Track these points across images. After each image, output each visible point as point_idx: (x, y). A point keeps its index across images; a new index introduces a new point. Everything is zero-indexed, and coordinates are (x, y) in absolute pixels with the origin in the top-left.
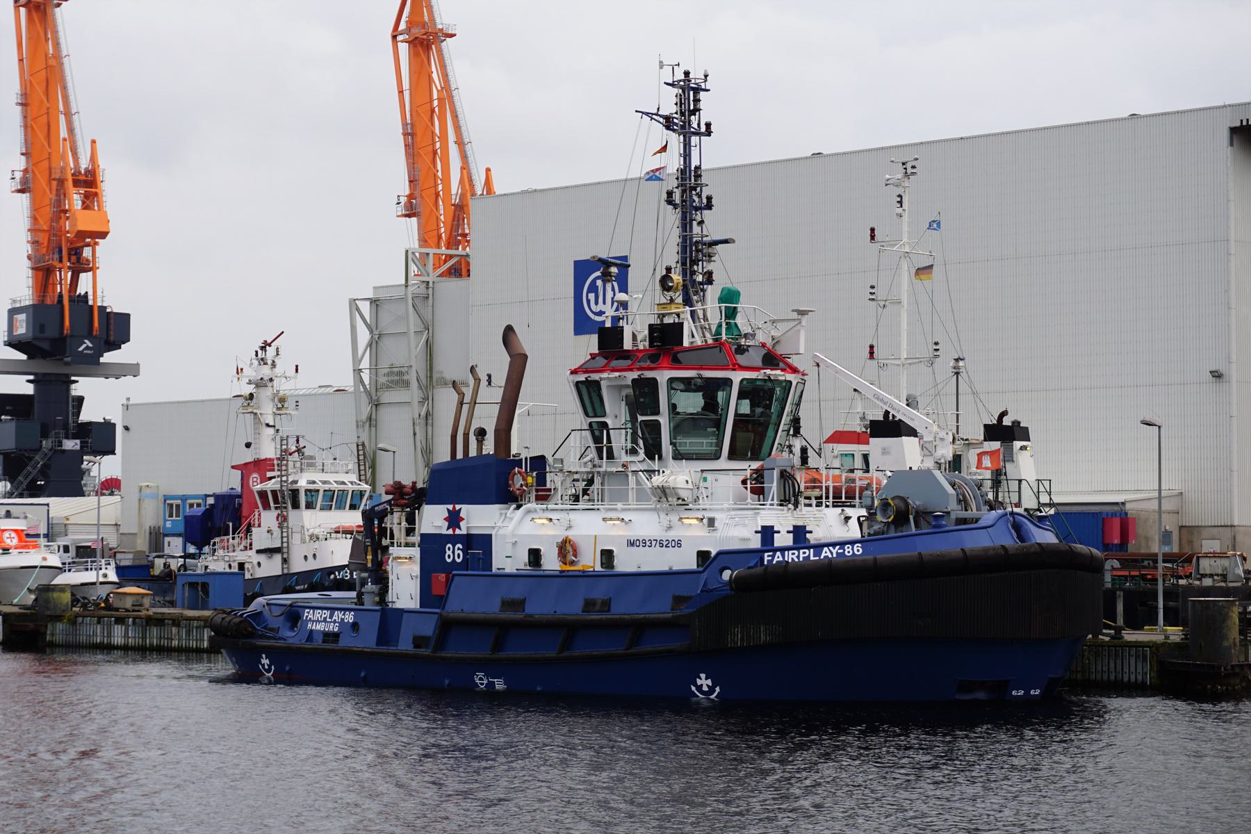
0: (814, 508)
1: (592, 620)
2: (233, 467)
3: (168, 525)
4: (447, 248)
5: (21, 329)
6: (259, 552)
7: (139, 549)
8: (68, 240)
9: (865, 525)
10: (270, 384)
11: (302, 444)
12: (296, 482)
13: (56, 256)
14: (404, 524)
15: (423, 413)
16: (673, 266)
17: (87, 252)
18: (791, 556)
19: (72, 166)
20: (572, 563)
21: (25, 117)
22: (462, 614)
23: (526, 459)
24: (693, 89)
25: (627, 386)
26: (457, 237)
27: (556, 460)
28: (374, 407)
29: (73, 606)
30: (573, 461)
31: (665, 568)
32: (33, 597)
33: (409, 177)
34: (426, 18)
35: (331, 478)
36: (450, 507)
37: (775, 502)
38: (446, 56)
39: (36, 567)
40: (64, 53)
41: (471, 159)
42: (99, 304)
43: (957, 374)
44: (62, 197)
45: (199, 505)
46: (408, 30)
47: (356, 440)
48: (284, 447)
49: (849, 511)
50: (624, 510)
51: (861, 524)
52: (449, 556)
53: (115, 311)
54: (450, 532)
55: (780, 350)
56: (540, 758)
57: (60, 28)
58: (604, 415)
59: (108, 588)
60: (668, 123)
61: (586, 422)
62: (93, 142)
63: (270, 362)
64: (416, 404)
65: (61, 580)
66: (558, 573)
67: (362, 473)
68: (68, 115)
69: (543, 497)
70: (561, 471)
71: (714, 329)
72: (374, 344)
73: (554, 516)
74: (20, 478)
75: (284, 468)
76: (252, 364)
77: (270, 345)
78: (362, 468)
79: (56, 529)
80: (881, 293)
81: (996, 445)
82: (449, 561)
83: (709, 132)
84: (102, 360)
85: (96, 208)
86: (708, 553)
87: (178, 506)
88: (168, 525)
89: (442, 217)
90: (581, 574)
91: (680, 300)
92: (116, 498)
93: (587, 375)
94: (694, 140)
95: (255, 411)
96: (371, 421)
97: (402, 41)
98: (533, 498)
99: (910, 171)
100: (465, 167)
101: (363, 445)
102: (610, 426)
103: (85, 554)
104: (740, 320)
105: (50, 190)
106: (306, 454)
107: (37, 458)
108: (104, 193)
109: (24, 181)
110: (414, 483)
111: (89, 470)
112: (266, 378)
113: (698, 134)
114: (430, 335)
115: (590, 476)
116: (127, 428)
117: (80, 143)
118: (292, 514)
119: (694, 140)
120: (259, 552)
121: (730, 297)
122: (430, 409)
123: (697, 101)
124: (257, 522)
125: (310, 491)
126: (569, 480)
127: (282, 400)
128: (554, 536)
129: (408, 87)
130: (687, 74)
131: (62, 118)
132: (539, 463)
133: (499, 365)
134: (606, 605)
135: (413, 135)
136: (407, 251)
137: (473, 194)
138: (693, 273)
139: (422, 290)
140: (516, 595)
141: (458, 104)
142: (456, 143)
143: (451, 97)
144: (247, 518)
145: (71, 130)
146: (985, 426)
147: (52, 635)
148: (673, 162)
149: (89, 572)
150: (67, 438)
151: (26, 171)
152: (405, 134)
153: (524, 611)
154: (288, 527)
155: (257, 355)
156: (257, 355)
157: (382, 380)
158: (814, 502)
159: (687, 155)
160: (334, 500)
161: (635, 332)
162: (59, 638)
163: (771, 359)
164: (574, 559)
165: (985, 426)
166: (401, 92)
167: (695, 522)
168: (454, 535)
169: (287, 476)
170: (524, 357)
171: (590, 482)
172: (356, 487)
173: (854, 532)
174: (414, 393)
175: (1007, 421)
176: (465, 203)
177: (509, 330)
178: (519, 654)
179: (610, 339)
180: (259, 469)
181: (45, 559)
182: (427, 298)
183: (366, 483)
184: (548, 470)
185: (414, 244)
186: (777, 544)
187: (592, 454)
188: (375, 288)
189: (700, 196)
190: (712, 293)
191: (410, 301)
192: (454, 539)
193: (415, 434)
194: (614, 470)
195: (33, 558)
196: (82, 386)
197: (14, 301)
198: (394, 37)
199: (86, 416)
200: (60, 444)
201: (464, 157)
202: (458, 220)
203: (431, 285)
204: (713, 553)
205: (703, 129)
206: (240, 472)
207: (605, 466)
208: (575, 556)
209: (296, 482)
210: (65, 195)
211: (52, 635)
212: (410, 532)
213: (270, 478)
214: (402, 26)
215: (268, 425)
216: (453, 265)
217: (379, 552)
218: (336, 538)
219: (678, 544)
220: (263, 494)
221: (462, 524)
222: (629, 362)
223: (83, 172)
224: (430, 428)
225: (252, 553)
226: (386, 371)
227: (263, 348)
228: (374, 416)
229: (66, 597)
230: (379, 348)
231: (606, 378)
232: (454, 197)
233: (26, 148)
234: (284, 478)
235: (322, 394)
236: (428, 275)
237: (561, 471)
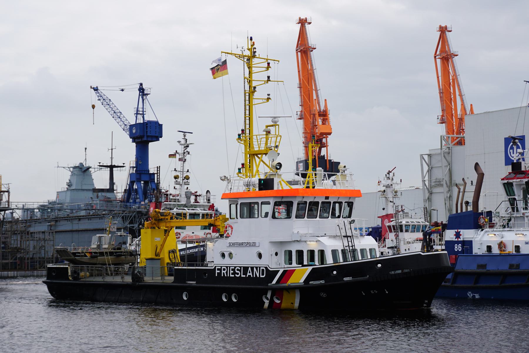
1: (512, 272)
2: (378, 217)
4: (457, 135)
6: (388, 248)
10: (391, 186)
12: (401, 222)
14: (439, 237)
15: (448, 196)
17: (324, 140)
19: (318, 109)
20: (504, 251)
21: (301, 92)
22: (462, 270)
23: (485, 212)
25: (523, 184)
26: (460, 130)
27: (496, 213)
28: (430, 194)
30: (503, 213)
33: (442, 109)
34: (447, 49)
35: (414, 220)
36: (456, 230)
38: (455, 63)
40: (314, 68)
41: (465, 101)
42: (329, 159)
44: (315, 120)
46: (440, 54)
47: (423, 206)
48: (397, 209)
52: (456, 249)
53: (334, 161)
54: (456, 240)
56: (64, 347)
58: (514, 195)
61: (507, 198)
62: (326, 100)
63: (391, 178)
64: (445, 192)
66: (499, 254)
67: (426, 218)
68: (316, 91)
69: (492, 226)
70: (498, 216)
72: (430, 171)
73: (496, 233)
75: (397, 217)
76: (384, 179)
77: (391, 172)
78: (426, 216)
82: (456, 250)
85: (327, 124)
89: (454, 123)
90: (508, 254)
93: (507, 181)
95: (386, 196)
96: (429, 199)
97: (438, 58)
98: (488, 226)
100: (463, 104)
101: (426, 208)
102: (517, 199)
105: (311, 118)
106: (405, 212)
108: (330, 119)
109: (301, 115)
110: (442, 222)
112: (390, 184)
115: (509, 218)
117: (321, 101)
118: (400, 234)
120: (388, 248)
122: (451, 194)
124: (387, 237)
125: (407, 225)
126: (502, 220)
127: (396, 192)
128: (496, 241)
129: (440, 75)
131: (314, 92)
132: (489, 213)
133: (475, 177)
134: (518, 266)
136: (441, 136)
137: (466, 114)
139: (447, 150)
140: (482, 263)
141: (459, 81)
142: (459, 95)
143: (457, 78)
144: (384, 236)
145: (317, 96)
151: (301, 111)
152: (440, 93)
153: (486, 269)
154: (399, 239)
155: (386, 176)
156: (386, 176)
157: (433, 184)
160: (415, 228)
164: (504, 249)
166: (438, 77)
167: (493, 235)
168: (458, 241)
169: (398, 220)
171: (510, 220)
172: (424, 224)
174: (445, 189)
176: (463, 117)
177: (477, 164)
178: (484, 285)
180: (388, 218)
182: (449, 153)
183: (428, 222)
184: (493, 216)
185: (444, 133)
187: (510, 210)
188: (430, 150)
192: (458, 242)
193: (445, 204)
194: (519, 216)
197: (298, 159)
198: (435, 57)
201: (462, 100)
202: (461, 124)
203: (450, 148)
206: (381, 219)
207: (515, 214)
208: (505, 248)
209: (401, 222)
210: (316, 120)
212: (440, 240)
213: (392, 221)
214: (438, 53)
215: (391, 201)
216: (459, 141)
217: (429, 248)
218: (417, 243)
220: (389, 227)
221: (461, 237)
222: (524, 175)
223: (322, 111)
224: (451, 201)
225: (386, 248)
226: (434, 181)
227: (388, 173)
228: (430, 198)
231: (515, 181)
232: (458, 115)
233: (302, 103)
234: (397, 221)
235: (411, 190)
236: (449, 145)
237: (498, 216)
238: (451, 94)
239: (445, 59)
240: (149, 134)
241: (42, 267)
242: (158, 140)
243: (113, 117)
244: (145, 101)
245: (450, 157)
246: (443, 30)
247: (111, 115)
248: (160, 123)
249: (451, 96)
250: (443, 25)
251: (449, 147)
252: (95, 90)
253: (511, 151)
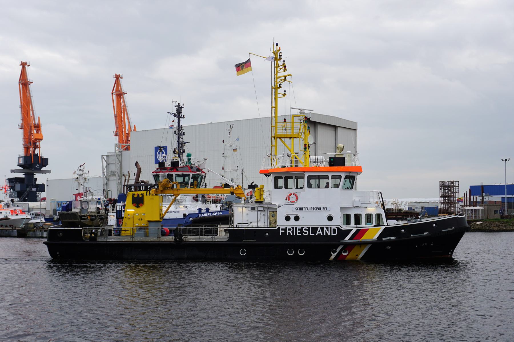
0: (209, 204)
2: (73, 195)
3: (58, 208)
5: (21, 162)
7: (51, 214)
8: (33, 141)
9: (222, 207)
11: (90, 189)
13: (30, 144)
14: (112, 208)
15: (119, 182)
16: (176, 148)
17: (37, 144)
18: (205, 215)
19: (34, 123)
24: (180, 107)
25: (166, 176)
26: (128, 141)
29: (34, 227)
31: (175, 218)
32: (24, 226)
34: (120, 89)
37: (201, 202)
39: (25, 219)
41: (131, 123)
42: (41, 156)
43: (242, 173)
45: (65, 204)
46: (116, 92)
49: (217, 205)
50: (165, 204)
51: (220, 208)
55: (200, 168)
57: (30, 90)
59: (43, 223)
60: (175, 115)
62: (39, 117)
63: (82, 170)
65: (31, 222)
68: (33, 111)
71: (185, 163)
72: (107, 166)
74: (21, 197)
79: (30, 210)
80: (225, 155)
81: (251, 190)
83: (184, 117)
84: (41, 169)
86: (186, 214)
87: (60, 204)
88: (58, 208)
91: (177, 156)
92: (45, 202)
94: (181, 119)
96: (107, 184)
99: (232, 127)
100: (129, 125)
101: (105, 189)
103: (37, 215)
104: (191, 161)
107: (26, 192)
109: (22, 126)
111: (39, 196)
113: (181, 118)
116: (47, 186)
119: (181, 119)
121: (189, 155)
123: (181, 110)
127: (85, 179)
130: (179, 104)
131: (31, 112)
133: (135, 170)
137: (131, 131)
138: (180, 150)
139: (119, 153)
141: (127, 110)
143: (126, 108)
145: (33, 114)
146: (249, 185)
147: (29, 234)
148: (176, 125)
149: (38, 220)
150: (33, 188)
151: (22, 124)
152: (115, 117)
157: (109, 174)
158: (209, 202)
159: (179, 123)
161: (168, 164)
162: (30, 235)
163: (198, 170)
165: (249, 185)
166: (114, 107)
167: (183, 207)
169: (86, 197)
170: (141, 169)
173: (219, 209)
175: (253, 184)
177: (137, 163)
179: (161, 165)
181: (27, 217)
182: (120, 155)
186: (202, 212)
189: (182, 132)
190: (185, 155)
195: (24, 216)
196: (37, 176)
198: (112, 94)
199: (37, 183)
200: (31, 189)
201: (129, 122)
204: (187, 214)
205: (183, 117)
211: (29, 234)
214: (114, 91)
215: (82, 185)
219: (179, 212)
227: (80, 167)
229: (32, 226)
231: (161, 174)
238: (122, 118)
246: (118, 77)
250: (118, 74)
253: (159, 155)
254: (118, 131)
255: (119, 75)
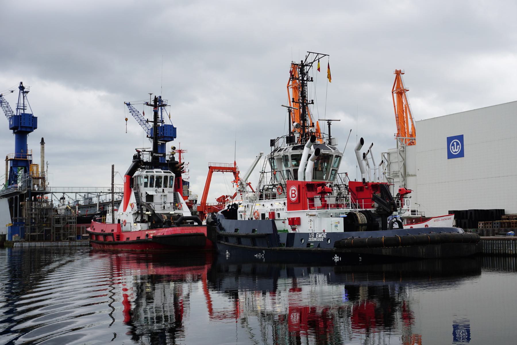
15: (403, 184)
34: (401, 86)
97: (395, 93)
114: (405, 162)
135: (398, 117)
139: (402, 149)
143: (408, 107)
152: (396, 117)
166: (395, 106)
182: (404, 151)
191: (398, 153)
198: (393, 92)
201: (412, 122)
203: (404, 147)
226: (392, 173)
230: (390, 167)
232: (410, 133)
238: (404, 118)
239: (400, 93)
240: (22, 125)
241: (66, 239)
242: (173, 140)
243: (140, 124)
244: (163, 110)
245: (404, 154)
246: (398, 73)
247: (139, 122)
248: (174, 127)
249: (404, 119)
250: (398, 70)
251: (404, 147)
252: (127, 105)
254: (400, 132)
255: (400, 71)
